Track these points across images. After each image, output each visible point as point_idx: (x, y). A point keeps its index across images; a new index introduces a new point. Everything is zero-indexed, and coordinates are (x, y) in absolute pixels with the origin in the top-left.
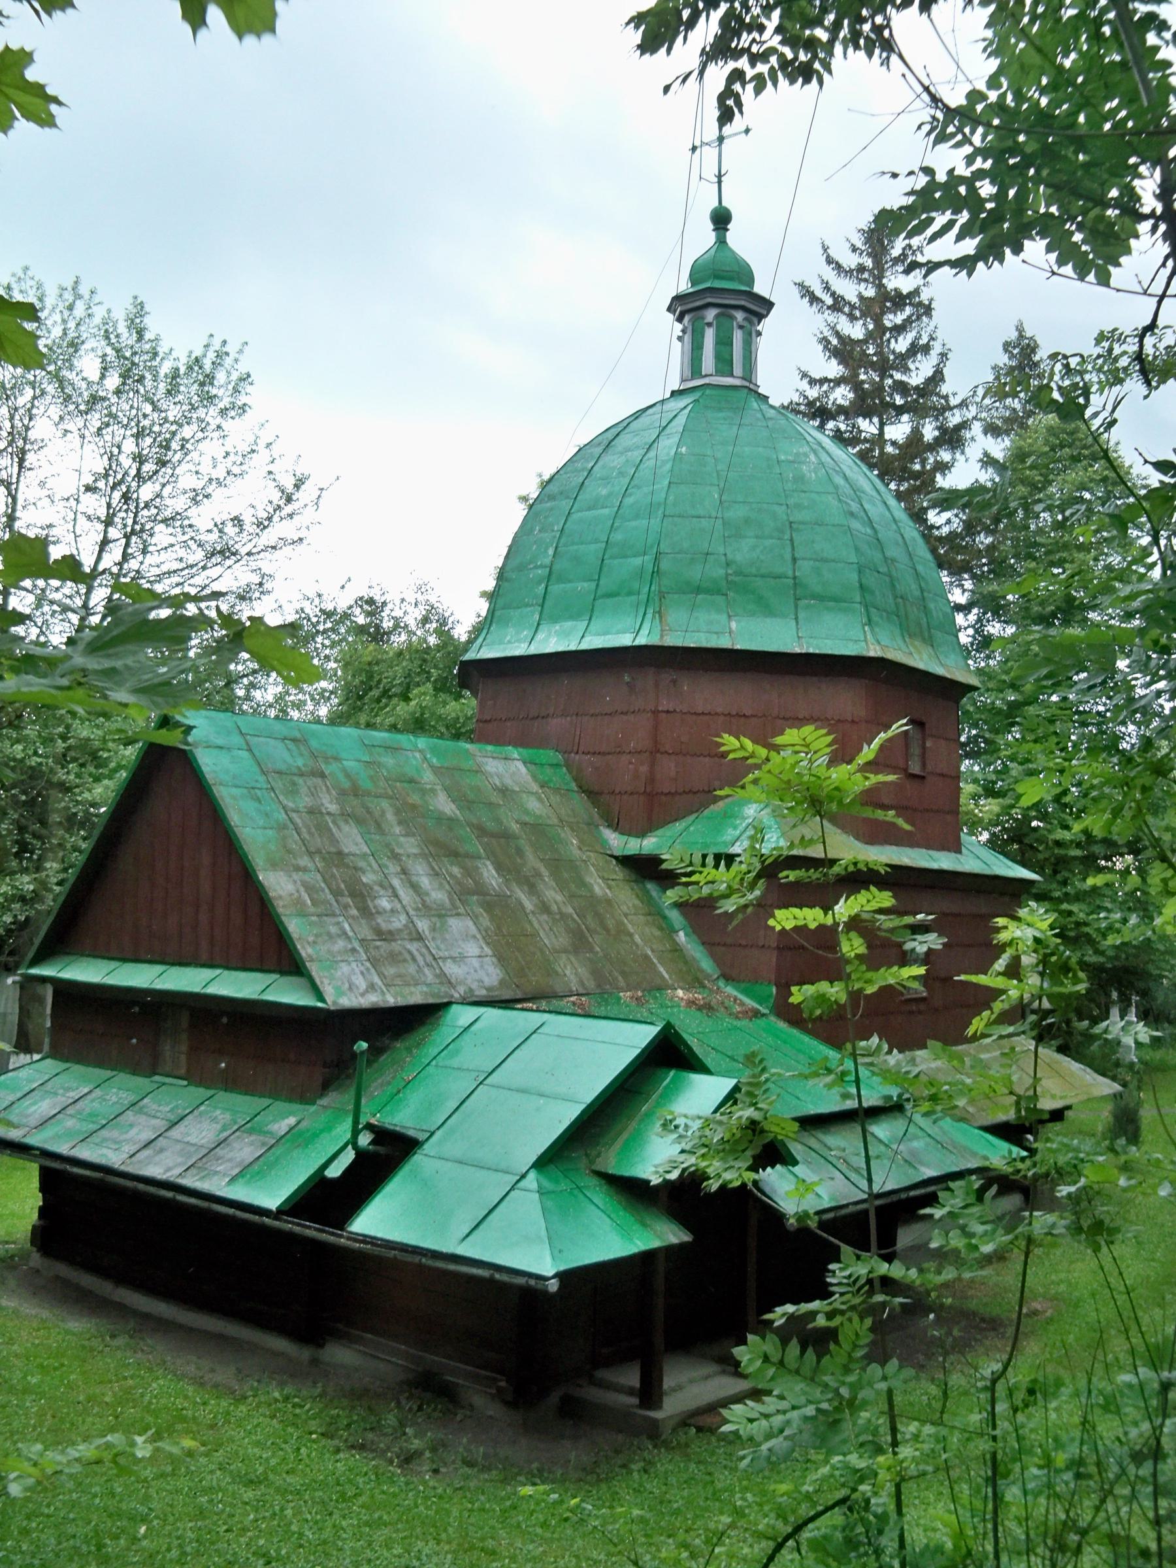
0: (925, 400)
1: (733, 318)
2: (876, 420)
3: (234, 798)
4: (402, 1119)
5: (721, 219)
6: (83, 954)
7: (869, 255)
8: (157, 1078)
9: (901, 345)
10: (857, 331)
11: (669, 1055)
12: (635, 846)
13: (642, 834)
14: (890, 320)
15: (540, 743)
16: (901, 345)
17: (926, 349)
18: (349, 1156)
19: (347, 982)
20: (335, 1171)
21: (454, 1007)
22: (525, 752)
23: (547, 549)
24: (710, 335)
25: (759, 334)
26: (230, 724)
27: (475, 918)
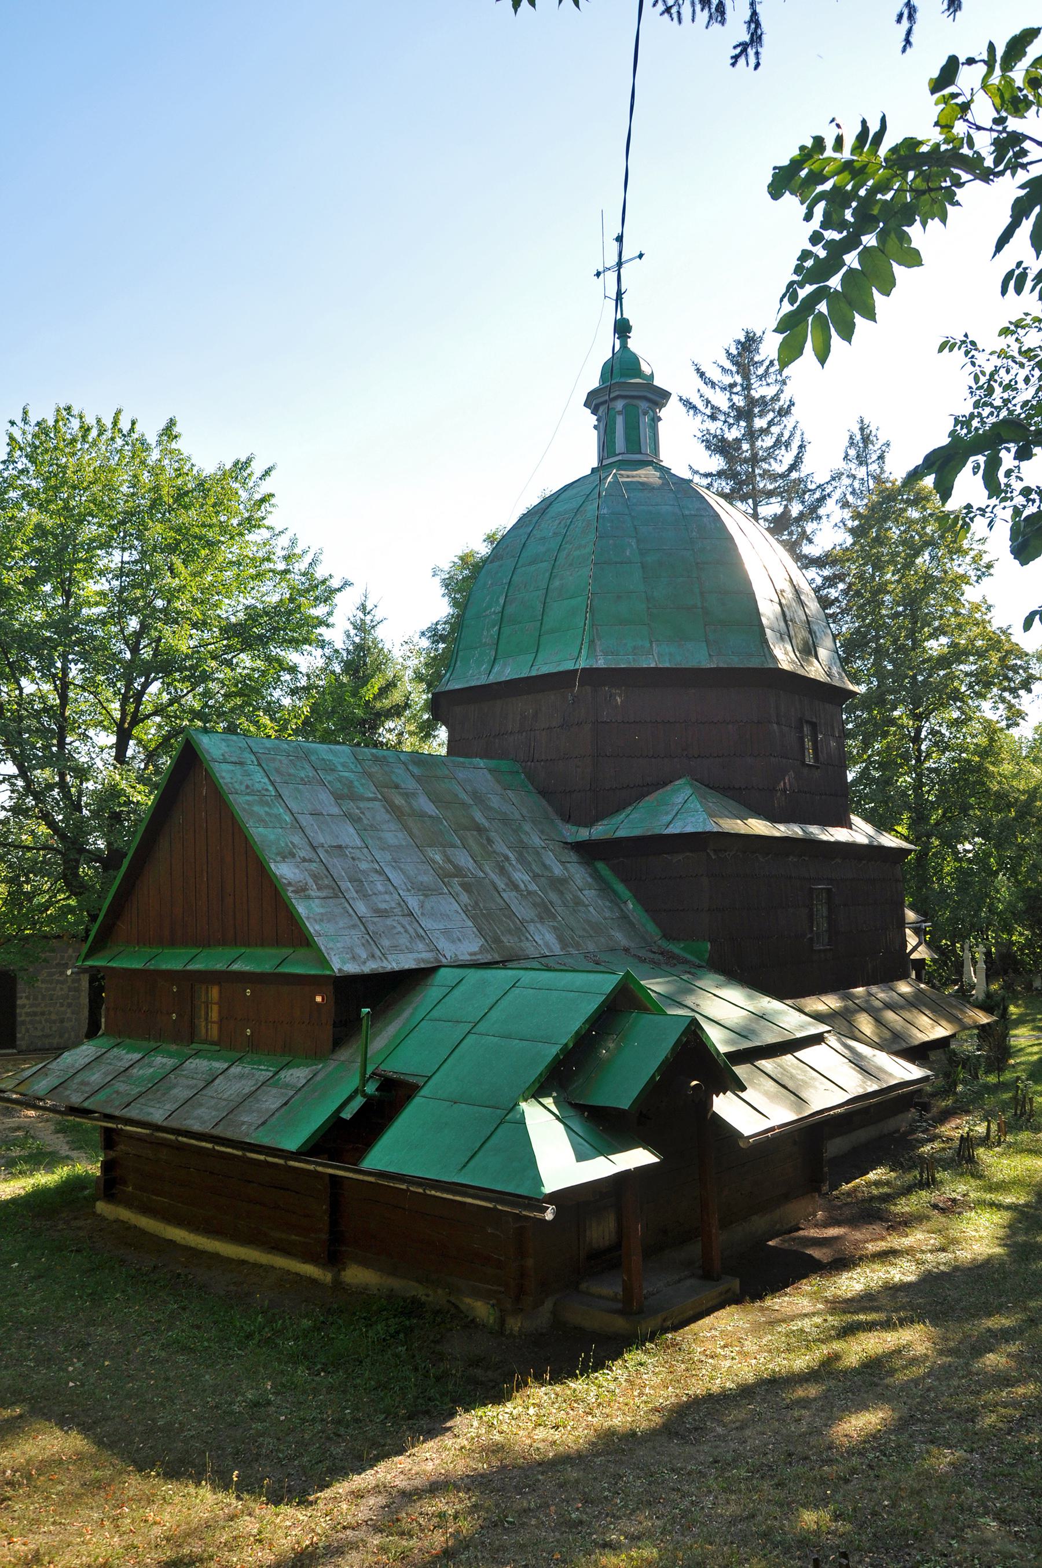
0: (793, 489)
1: (636, 407)
2: (750, 501)
3: (248, 803)
4: (399, 1065)
5: (622, 328)
7: (738, 373)
8: (194, 1046)
9: (768, 441)
10: (733, 434)
12: (584, 834)
13: (589, 823)
14: (759, 423)
15: (503, 755)
16: (768, 441)
17: (787, 445)
18: (359, 1102)
19: (345, 955)
20: (347, 1115)
21: (442, 970)
22: (493, 763)
23: (498, 598)
24: (620, 421)
25: (660, 419)
26: (243, 744)
27: (455, 897)
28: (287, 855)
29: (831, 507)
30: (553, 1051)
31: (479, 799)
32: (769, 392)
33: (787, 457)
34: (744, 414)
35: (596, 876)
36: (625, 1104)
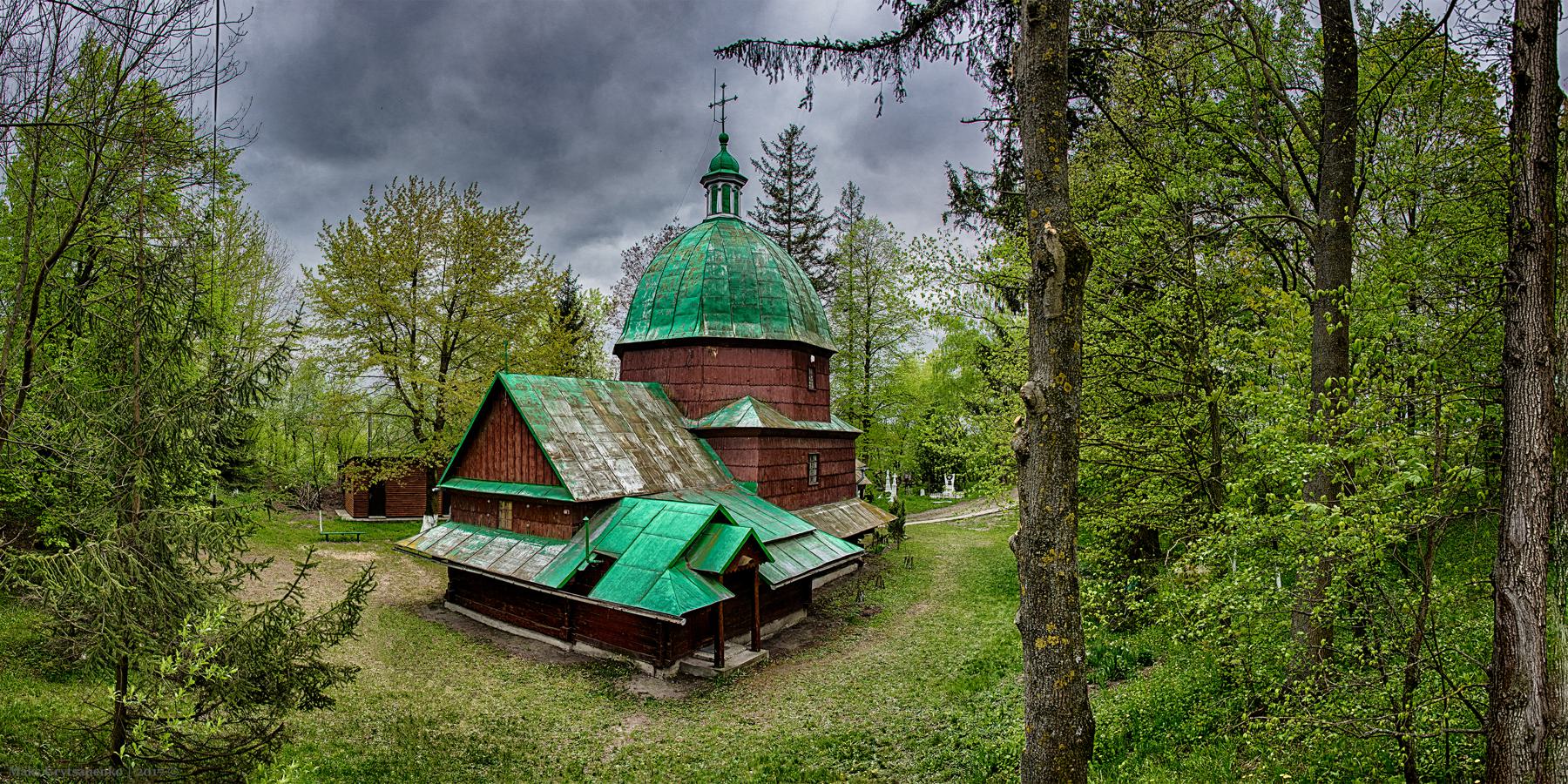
0: (810, 220)
4: (611, 545)
6: (463, 476)
11: (720, 518)
12: (694, 424)
13: (698, 419)
14: (796, 180)
18: (586, 564)
19: (579, 490)
28: (550, 439)
29: (833, 232)
30: (682, 544)
31: (641, 405)
32: (802, 163)
33: (810, 203)
34: (787, 174)
35: (701, 446)
36: (719, 570)
